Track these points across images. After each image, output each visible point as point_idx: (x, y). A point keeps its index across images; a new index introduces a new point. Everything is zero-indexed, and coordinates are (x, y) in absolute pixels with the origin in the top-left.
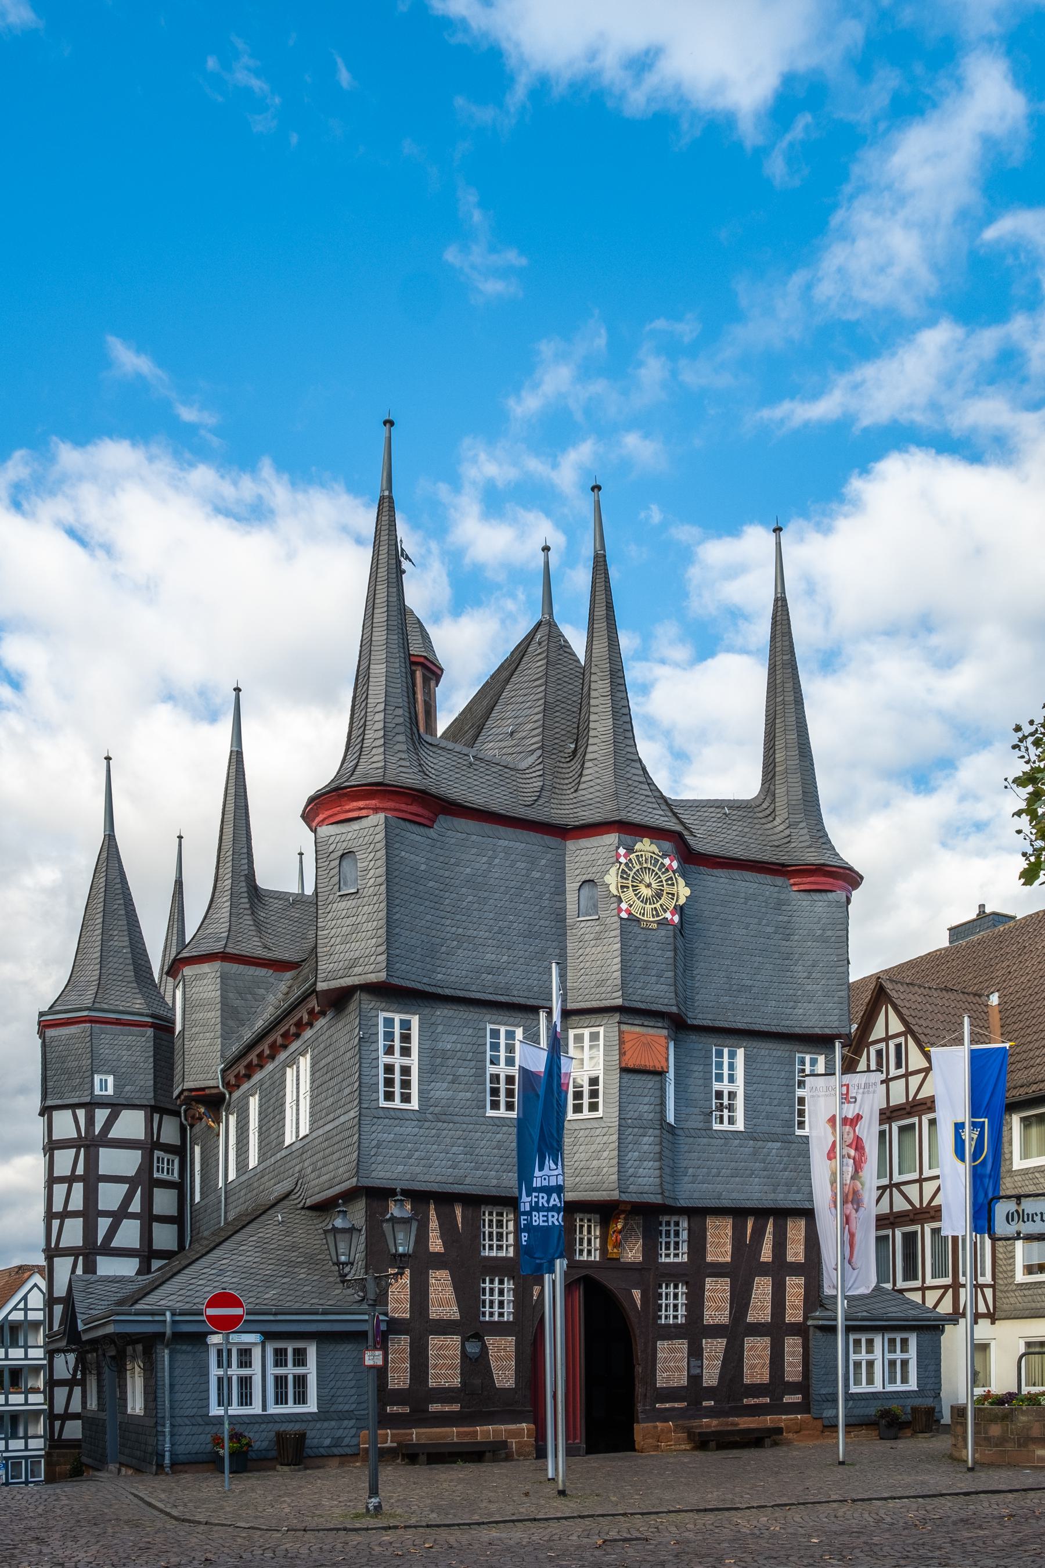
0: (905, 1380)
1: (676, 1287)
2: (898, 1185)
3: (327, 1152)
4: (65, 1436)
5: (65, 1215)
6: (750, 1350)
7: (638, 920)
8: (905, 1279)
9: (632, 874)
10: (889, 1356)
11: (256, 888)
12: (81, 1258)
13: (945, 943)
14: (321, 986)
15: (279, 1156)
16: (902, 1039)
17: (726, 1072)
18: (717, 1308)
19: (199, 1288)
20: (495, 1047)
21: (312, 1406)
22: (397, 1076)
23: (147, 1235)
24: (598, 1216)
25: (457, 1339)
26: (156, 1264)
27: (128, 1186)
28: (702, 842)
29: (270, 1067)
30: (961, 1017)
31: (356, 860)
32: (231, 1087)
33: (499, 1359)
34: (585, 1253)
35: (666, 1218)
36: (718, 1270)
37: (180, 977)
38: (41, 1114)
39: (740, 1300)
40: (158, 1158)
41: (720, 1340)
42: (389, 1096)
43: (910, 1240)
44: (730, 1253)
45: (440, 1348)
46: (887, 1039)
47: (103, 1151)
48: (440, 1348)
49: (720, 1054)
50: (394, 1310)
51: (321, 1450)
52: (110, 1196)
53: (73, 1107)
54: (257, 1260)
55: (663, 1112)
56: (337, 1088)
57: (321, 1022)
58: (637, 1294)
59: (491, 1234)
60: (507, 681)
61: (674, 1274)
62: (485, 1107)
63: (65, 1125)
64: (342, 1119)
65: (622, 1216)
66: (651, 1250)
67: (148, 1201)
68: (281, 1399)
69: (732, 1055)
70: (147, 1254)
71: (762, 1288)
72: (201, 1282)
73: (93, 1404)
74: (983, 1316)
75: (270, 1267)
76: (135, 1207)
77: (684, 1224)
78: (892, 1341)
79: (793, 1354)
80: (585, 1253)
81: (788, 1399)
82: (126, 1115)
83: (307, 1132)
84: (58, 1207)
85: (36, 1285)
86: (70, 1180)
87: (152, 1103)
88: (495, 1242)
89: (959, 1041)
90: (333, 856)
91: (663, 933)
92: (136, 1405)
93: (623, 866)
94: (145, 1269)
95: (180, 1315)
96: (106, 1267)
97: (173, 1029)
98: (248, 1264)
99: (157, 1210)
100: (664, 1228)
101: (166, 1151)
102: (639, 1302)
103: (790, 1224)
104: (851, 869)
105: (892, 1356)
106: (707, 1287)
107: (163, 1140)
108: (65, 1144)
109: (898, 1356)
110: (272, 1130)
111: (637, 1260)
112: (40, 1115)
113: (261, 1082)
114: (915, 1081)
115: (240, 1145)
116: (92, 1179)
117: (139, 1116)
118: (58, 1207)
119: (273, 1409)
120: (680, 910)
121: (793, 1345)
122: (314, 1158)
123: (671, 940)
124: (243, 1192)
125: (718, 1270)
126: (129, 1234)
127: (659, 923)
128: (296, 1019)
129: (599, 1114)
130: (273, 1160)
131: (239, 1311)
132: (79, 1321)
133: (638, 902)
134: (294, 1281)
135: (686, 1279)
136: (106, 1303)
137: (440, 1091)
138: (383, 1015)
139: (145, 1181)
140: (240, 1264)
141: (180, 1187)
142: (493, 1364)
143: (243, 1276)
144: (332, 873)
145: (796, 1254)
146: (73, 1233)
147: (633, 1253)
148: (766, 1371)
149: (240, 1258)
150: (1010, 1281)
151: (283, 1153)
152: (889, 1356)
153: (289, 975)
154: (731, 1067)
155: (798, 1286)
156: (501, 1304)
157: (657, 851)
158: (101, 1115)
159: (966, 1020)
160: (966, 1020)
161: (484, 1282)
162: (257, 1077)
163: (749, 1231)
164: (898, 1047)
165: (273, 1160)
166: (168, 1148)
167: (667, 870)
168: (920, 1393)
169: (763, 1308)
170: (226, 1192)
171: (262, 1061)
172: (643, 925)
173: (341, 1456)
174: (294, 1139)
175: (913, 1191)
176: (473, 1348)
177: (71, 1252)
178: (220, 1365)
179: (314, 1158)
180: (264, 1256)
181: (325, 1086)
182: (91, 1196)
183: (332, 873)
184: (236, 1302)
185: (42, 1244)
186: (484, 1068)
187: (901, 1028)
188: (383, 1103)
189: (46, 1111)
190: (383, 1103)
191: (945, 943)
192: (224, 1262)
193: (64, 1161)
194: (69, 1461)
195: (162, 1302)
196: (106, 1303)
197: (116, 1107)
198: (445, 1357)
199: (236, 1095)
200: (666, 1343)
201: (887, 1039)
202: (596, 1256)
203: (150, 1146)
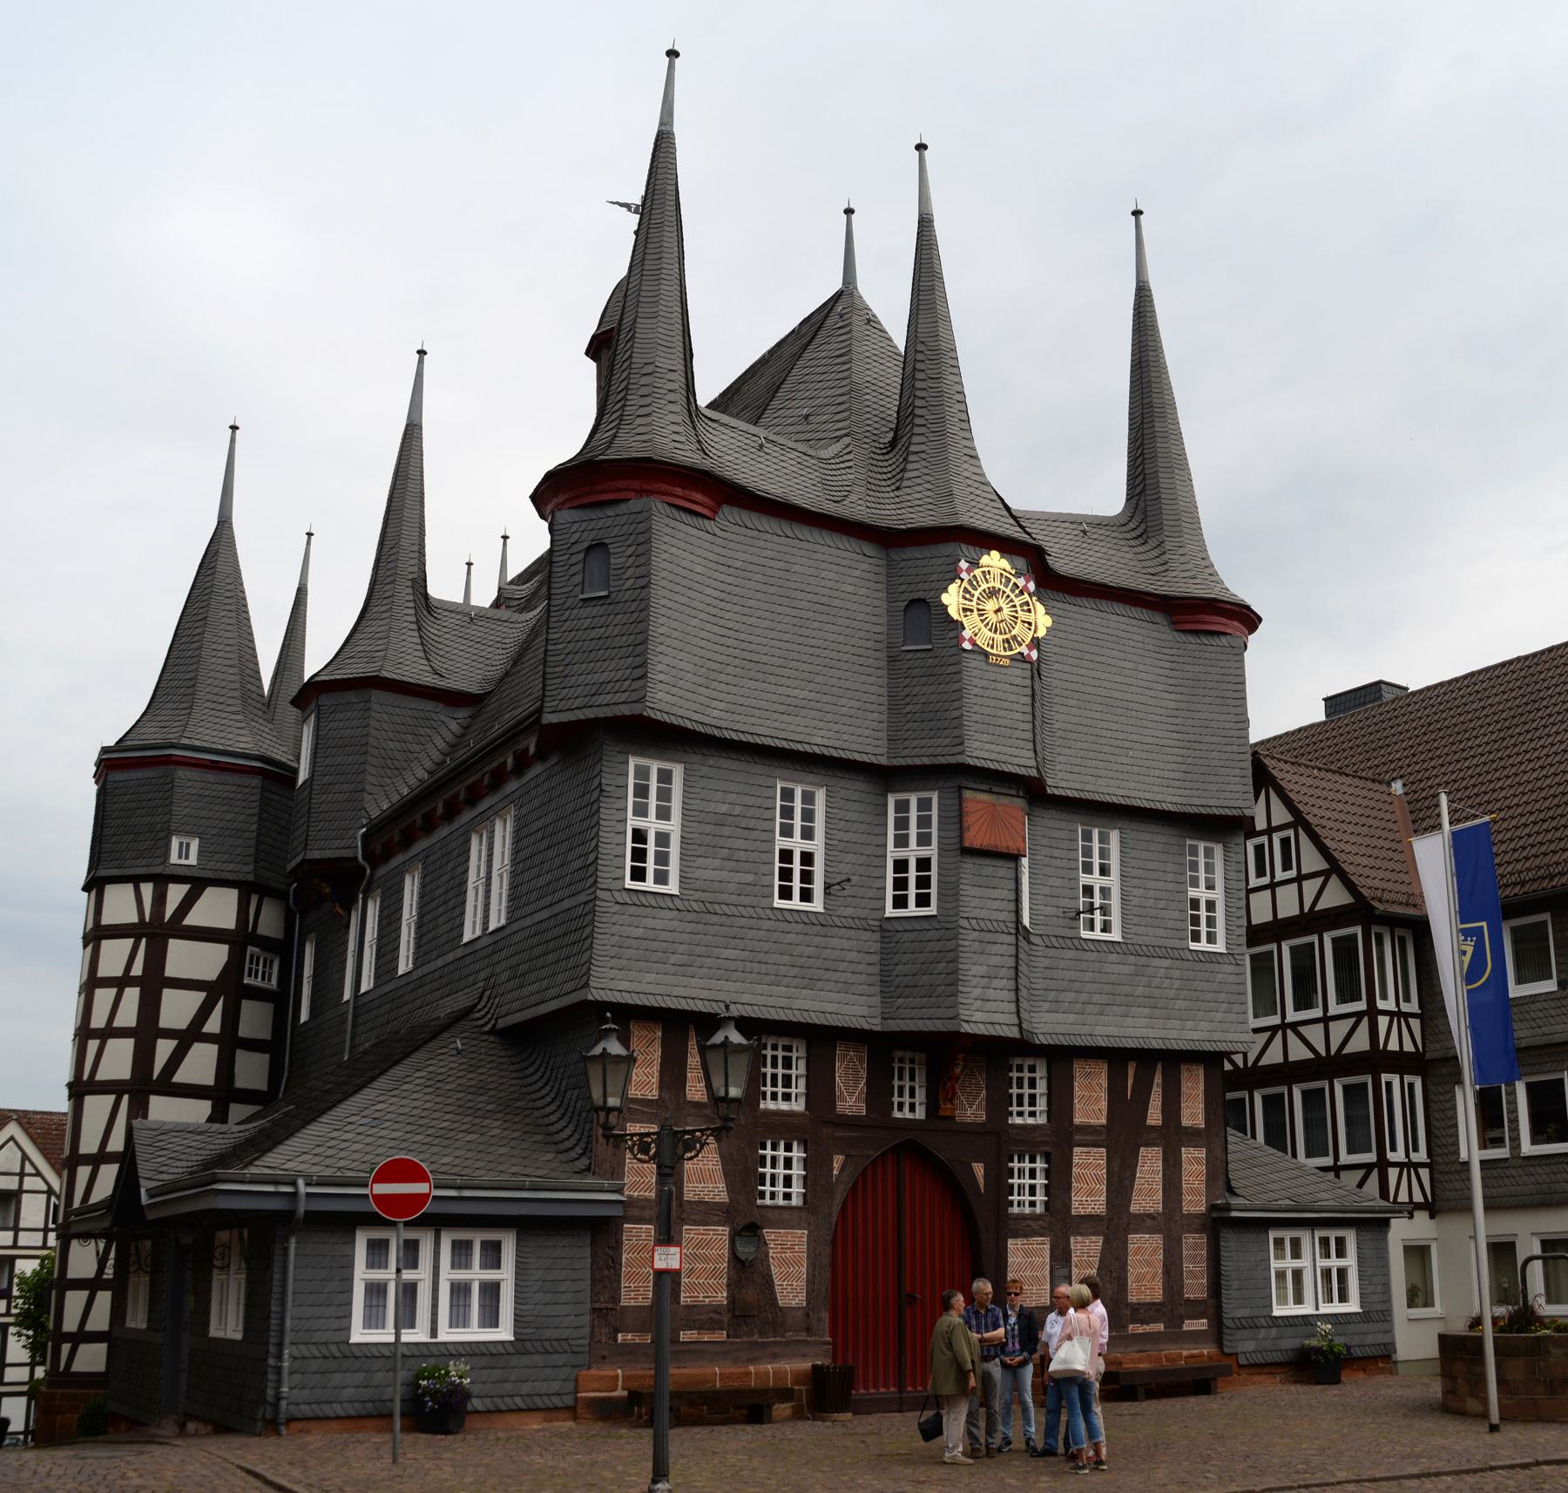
0: (1343, 1298)
1: (788, 1148)
2: (1294, 1026)
3: (536, 952)
4: (77, 1367)
5: (110, 1032)
6: (1136, 1254)
7: (986, 654)
8: (1350, 1151)
9: (977, 594)
10: (1323, 1263)
11: (426, 596)
12: (126, 1097)
13: (1320, 716)
14: (548, 718)
15: (450, 957)
16: (1291, 833)
17: (1096, 861)
18: (1089, 1198)
19: (343, 1145)
20: (787, 812)
21: (504, 1333)
22: (912, 874)
23: (225, 1067)
24: (923, 1056)
25: (724, 1231)
26: (237, 1111)
27: (204, 994)
28: (1062, 562)
29: (443, 832)
30: (1436, 796)
31: (609, 555)
32: (375, 860)
33: (785, 1263)
34: (907, 1108)
35: (1018, 1061)
36: (1091, 1135)
37: (313, 705)
38: (86, 888)
39: (1120, 1183)
40: (252, 957)
41: (1093, 1238)
42: (900, 902)
43: (1313, 1100)
44: (1105, 1113)
45: (699, 1245)
46: (1270, 831)
47: (174, 944)
48: (699, 1245)
49: (1087, 837)
50: (634, 1186)
51: (518, 1400)
52: (177, 1009)
53: (136, 880)
54: (427, 1105)
55: (1018, 912)
56: (558, 862)
57: (537, 769)
58: (979, 1169)
59: (774, 1076)
60: (798, 356)
61: (1028, 1143)
62: (772, 895)
63: (121, 905)
64: (566, 904)
65: (961, 1056)
66: (999, 1104)
67: (231, 1019)
68: (459, 1319)
69: (1104, 839)
70: (222, 1094)
71: (1150, 1163)
72: (346, 1136)
73: (137, 1320)
74: (1419, 1206)
75: (448, 1117)
76: (213, 1025)
77: (1041, 1073)
78: (1325, 1242)
79: (1193, 1259)
80: (907, 1108)
81: (1190, 1325)
82: (210, 894)
83: (503, 922)
84: (98, 1021)
85: (12, 1138)
86: (121, 983)
87: (251, 878)
88: (780, 1090)
89: (1437, 827)
90: (575, 548)
91: (1018, 672)
92: (227, 1324)
93: (965, 584)
94: (219, 1116)
95: (318, 1184)
96: (162, 1109)
97: (295, 780)
98: (415, 1112)
99: (244, 1031)
100: (1014, 1075)
101: (263, 948)
102: (981, 1181)
103: (1184, 1075)
104: (1248, 608)
105: (1326, 1263)
106: (1076, 1160)
107: (261, 931)
108: (117, 932)
109: (1334, 1263)
110: (441, 920)
111: (979, 1120)
112: (84, 889)
113: (427, 853)
114: (1311, 887)
115: (385, 941)
116: (154, 983)
117: (232, 895)
118: (98, 1021)
119: (446, 1335)
120: (1036, 643)
121: (1194, 1246)
122: (514, 961)
123: (1028, 682)
124: (383, 1010)
125: (1091, 1135)
126: (200, 1065)
127: (1012, 658)
128: (495, 764)
129: (932, 910)
130: (440, 962)
131: (421, 1188)
132: (143, 1191)
133: (985, 631)
134: (483, 1139)
135: (1046, 1149)
136: (184, 1164)
137: (710, 870)
138: (633, 762)
139: (226, 989)
140: (403, 1110)
141: (282, 1000)
142: (774, 1270)
143: (409, 1128)
144: (573, 570)
145: (1194, 1116)
146: (118, 1061)
147: (972, 1111)
148: (1158, 1283)
149: (404, 1102)
150: (1452, 1158)
151: (459, 953)
152: (1323, 1263)
153: (463, 713)
154: (1104, 854)
155: (1198, 1160)
156: (788, 1181)
157: (1008, 567)
158: (176, 893)
159: (1444, 799)
160: (1444, 799)
161: (764, 1148)
162: (420, 846)
163: (1130, 1083)
164: (1285, 842)
165: (440, 962)
166: (265, 943)
167: (1022, 593)
168: (1365, 1316)
169: (1150, 1192)
170: (355, 1008)
171: (430, 826)
172: (992, 660)
173: (548, 1409)
174: (478, 933)
175: (1315, 1034)
176: (746, 1250)
177: (113, 1088)
178: (371, 1265)
179: (514, 961)
180: (439, 1099)
181: (537, 860)
182: (149, 1007)
183: (573, 570)
184: (417, 1174)
185: (67, 1075)
186: (772, 841)
187: (1289, 818)
188: (629, 884)
189: (95, 885)
190: (629, 884)
191: (1320, 716)
192: (379, 1107)
193: (114, 956)
194: (72, 1413)
195: (289, 1165)
196: (184, 1164)
197: (197, 884)
198: (706, 1259)
199: (382, 871)
200: (1019, 1241)
201: (1270, 831)
202: (920, 1113)
203: (238, 939)
